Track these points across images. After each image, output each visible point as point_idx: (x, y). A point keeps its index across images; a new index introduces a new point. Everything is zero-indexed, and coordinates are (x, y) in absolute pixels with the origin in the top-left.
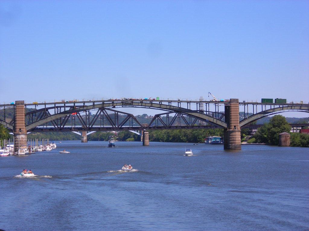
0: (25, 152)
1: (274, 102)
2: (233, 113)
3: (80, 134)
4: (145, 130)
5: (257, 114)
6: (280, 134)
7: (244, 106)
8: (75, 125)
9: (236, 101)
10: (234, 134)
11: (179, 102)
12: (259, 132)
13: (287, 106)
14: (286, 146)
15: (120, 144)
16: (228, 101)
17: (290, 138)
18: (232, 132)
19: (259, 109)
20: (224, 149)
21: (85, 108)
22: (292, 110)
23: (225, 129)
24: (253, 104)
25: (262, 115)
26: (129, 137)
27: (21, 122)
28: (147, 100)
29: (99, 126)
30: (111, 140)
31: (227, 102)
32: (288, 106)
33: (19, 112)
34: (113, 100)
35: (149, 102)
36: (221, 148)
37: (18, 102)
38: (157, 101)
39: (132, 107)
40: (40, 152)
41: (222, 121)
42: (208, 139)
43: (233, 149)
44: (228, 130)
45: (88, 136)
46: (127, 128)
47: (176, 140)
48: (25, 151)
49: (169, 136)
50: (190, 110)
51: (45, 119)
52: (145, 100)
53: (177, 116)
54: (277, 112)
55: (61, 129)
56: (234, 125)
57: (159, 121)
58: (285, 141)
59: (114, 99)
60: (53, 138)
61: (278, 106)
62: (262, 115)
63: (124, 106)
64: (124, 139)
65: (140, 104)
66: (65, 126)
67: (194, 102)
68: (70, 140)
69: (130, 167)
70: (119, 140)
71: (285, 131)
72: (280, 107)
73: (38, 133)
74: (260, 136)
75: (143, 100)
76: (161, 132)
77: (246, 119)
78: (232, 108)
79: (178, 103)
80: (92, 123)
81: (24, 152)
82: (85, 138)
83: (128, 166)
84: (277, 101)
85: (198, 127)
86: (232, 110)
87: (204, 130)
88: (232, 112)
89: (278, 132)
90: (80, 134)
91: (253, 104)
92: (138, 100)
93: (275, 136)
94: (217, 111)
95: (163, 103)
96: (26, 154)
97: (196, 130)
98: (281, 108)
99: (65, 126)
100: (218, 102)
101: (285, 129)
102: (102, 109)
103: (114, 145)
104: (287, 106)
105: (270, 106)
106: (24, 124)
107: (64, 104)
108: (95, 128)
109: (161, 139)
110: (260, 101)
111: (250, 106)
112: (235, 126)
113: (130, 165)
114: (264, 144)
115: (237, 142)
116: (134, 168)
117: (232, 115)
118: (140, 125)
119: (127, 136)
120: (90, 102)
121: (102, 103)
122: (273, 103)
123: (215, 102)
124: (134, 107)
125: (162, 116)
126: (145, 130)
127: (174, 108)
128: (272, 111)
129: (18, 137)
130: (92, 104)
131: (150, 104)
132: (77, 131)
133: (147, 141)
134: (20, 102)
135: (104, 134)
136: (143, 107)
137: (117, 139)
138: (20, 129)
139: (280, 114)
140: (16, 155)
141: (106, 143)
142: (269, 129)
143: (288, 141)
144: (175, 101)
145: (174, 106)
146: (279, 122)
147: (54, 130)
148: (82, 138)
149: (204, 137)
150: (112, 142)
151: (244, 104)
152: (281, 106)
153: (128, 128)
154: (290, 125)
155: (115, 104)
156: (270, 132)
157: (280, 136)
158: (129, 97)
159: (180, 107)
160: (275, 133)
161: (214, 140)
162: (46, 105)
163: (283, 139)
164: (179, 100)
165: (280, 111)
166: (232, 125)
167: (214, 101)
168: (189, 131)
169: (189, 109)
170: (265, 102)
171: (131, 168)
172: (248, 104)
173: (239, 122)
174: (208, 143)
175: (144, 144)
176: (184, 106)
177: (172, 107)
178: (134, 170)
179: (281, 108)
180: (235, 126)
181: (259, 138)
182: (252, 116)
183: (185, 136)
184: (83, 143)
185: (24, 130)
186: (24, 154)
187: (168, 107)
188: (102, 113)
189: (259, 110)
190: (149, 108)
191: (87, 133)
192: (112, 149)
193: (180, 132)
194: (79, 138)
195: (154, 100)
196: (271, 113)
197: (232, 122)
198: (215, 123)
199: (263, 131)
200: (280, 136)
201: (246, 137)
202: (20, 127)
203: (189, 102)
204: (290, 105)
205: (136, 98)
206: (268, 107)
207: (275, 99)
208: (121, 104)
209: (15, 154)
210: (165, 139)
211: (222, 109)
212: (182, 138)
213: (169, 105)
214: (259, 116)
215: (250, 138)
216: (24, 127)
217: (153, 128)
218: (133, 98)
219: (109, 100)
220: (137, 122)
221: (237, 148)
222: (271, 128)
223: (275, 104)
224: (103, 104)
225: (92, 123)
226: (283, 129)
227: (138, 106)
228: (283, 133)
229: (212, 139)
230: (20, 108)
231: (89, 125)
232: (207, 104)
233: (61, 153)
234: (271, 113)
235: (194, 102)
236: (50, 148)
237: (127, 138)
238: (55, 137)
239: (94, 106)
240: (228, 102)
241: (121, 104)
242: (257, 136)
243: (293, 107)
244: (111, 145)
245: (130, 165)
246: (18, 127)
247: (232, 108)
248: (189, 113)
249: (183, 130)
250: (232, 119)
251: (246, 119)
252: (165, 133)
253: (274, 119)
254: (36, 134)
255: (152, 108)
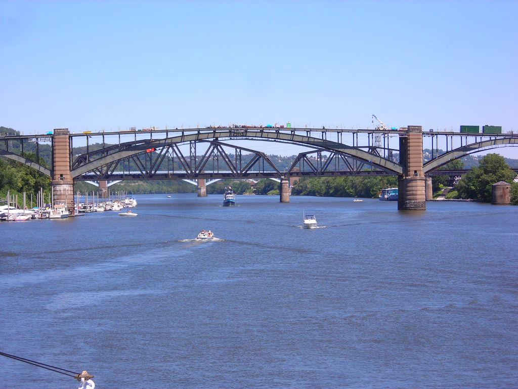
0: (61, 214)
1: (481, 131)
2: (412, 150)
3: (97, 185)
4: (283, 177)
5: (452, 151)
6: (494, 184)
7: (431, 137)
8: (168, 171)
9: (418, 130)
10: (414, 184)
11: (324, 131)
12: (464, 182)
13: (502, 137)
14: (504, 204)
15: (243, 199)
16: (404, 130)
17: (510, 192)
18: (411, 180)
19: (456, 143)
20: (398, 209)
21: (169, 141)
22: (511, 145)
23: (400, 176)
24: (446, 134)
25: (462, 153)
26: (272, 189)
27: (63, 165)
28: (271, 127)
29: (211, 172)
30: (228, 194)
31: (403, 131)
32: (505, 138)
33: (60, 147)
34: (215, 128)
35: (275, 132)
36: (394, 206)
37: (59, 131)
38: (287, 129)
39: (246, 139)
40: (100, 213)
41: (394, 163)
42: (384, 193)
43: (413, 208)
44: (404, 178)
45: (207, 186)
46: (255, 175)
47: (339, 193)
48: (61, 212)
49: (329, 188)
50: (341, 144)
51: (103, 159)
52: (267, 127)
53: (333, 156)
54: (486, 148)
55: (151, 177)
56: (415, 169)
57: (304, 161)
58: (502, 196)
59: (216, 127)
60: (162, 189)
61: (487, 138)
62: (462, 153)
63: (232, 138)
64: (264, 192)
65: (260, 135)
66: (158, 172)
67: (348, 131)
68: (187, 193)
69: (209, 234)
70: (257, 192)
71: (504, 179)
72: (491, 140)
73: (141, 183)
74: (465, 187)
75: (263, 128)
76: (318, 182)
77: (435, 159)
78: (411, 141)
79: (323, 132)
80: (155, 167)
81: (59, 213)
82: (203, 190)
83: (207, 233)
84: (486, 130)
85: (366, 173)
86: (411, 144)
87: (380, 178)
88: (411, 148)
89: (492, 181)
90: (97, 185)
91: (446, 135)
92: (255, 127)
93: (488, 187)
94: (435, 148)
95: (296, 133)
96: (63, 217)
97: (369, 178)
98: (493, 142)
99: (158, 172)
100: (389, 130)
101: (503, 176)
102: (216, 144)
103: (233, 203)
104: (502, 137)
105: (474, 138)
106: (68, 168)
107: (181, 133)
108: (117, 175)
109: (318, 192)
110: (458, 131)
111: (442, 138)
112: (416, 172)
113: (210, 231)
114: (471, 201)
115: (418, 197)
116: (216, 236)
117: (411, 152)
118: (276, 170)
119: (269, 185)
120: (177, 130)
121: (196, 132)
122: (480, 132)
123: (383, 130)
124: (250, 139)
125: (309, 156)
126: (283, 177)
127: (316, 140)
128: (477, 146)
129: (58, 188)
130: (180, 134)
131: (276, 134)
132: (191, 179)
133: (287, 195)
134: (61, 131)
135: (236, 183)
136: (264, 139)
137: (255, 192)
138: (61, 175)
139: (491, 152)
140: (46, 218)
141: (221, 198)
142: (478, 177)
143: (507, 196)
144: (317, 130)
145: (315, 138)
146: (495, 166)
147: (140, 177)
148: (199, 190)
149: (379, 189)
150: (230, 198)
151: (432, 134)
152: (493, 138)
153: (257, 174)
154: (512, 170)
155: (217, 135)
156: (480, 181)
157: (494, 188)
158: (240, 124)
159: (326, 140)
160: (487, 183)
161: (393, 194)
162: (105, 136)
163: (498, 193)
164: (324, 128)
165: (490, 147)
166: (411, 169)
167: (382, 129)
168: (358, 180)
169: (340, 142)
170: (467, 130)
171: (211, 236)
172: (437, 134)
173: (422, 165)
174: (383, 199)
175: (281, 201)
176: (332, 137)
177: (312, 140)
178: (215, 239)
179: (493, 142)
180: (416, 172)
181: (464, 191)
182: (444, 154)
183: (352, 187)
184: (199, 198)
185: (68, 177)
186: (60, 217)
187: (306, 140)
188: (215, 151)
189: (457, 145)
190: (275, 141)
191: (108, 183)
192: (230, 209)
193: (345, 181)
194: (196, 190)
195: (282, 127)
196: (477, 150)
197: (411, 164)
198: (383, 167)
199: (469, 179)
200: (494, 188)
201: (443, 188)
202: (61, 173)
203: (340, 132)
204: (507, 137)
205: (254, 125)
206: (471, 140)
207: (483, 127)
208: (228, 134)
209: (43, 217)
210: (323, 192)
211: (394, 143)
212: (348, 191)
213: (307, 137)
214: (456, 154)
215: (451, 191)
216: (68, 172)
217: (296, 174)
218: (248, 125)
219: (209, 128)
220: (272, 165)
221: (418, 208)
222: (482, 175)
223: (483, 135)
224: (199, 133)
225: (155, 167)
226: (500, 177)
227: (256, 138)
228: (499, 183)
229: (389, 192)
230: (62, 140)
231: (196, 169)
232: (340, 134)
233: (121, 215)
234: (477, 150)
235: (348, 131)
236: (118, 206)
237: (269, 191)
238: (165, 188)
239: (183, 138)
240: (405, 131)
241: (228, 134)
242: (461, 187)
243: (513, 140)
244: (227, 203)
245: (210, 231)
246: (58, 173)
247: (411, 141)
248: (339, 150)
249: (350, 178)
250: (411, 160)
251: (435, 159)
252: (323, 183)
253: (486, 160)
254: (137, 184)
255: (279, 140)
